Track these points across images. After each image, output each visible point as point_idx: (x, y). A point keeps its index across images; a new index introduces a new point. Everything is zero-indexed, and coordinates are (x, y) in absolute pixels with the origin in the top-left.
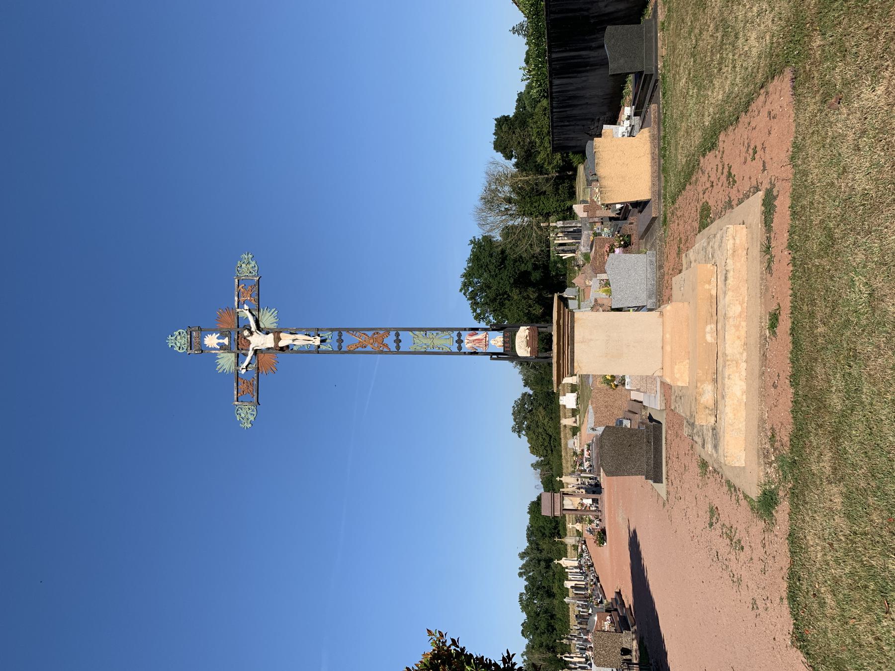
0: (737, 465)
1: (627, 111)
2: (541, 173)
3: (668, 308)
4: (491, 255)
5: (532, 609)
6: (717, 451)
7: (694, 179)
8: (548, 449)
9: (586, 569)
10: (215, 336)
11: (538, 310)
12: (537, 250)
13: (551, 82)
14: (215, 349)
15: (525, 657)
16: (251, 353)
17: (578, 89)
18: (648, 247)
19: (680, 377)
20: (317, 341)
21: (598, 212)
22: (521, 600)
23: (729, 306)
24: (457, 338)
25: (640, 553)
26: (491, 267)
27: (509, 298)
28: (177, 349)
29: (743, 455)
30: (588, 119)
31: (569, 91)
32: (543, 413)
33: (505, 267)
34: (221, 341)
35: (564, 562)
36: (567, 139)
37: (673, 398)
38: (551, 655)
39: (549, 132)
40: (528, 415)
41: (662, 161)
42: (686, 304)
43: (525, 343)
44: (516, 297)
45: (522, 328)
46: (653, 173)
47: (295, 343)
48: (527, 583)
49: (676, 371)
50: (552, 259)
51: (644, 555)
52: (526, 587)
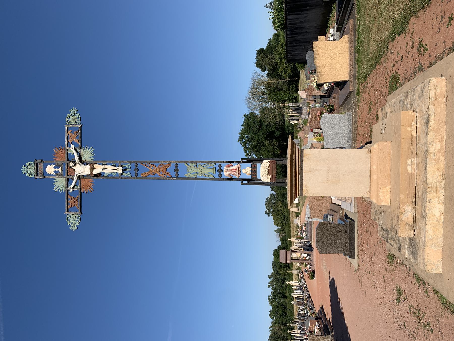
0: (435, 272)
1: (332, 31)
2: (281, 79)
3: (375, 146)
4: (254, 123)
5: (275, 304)
6: (415, 258)
7: (383, 59)
8: (284, 222)
9: (303, 288)
10: (53, 166)
11: (279, 152)
12: (279, 120)
13: (286, 18)
14: (53, 175)
15: (271, 329)
16: (75, 178)
17: (302, 22)
18: (346, 110)
19: (383, 198)
20: (120, 170)
21: (313, 92)
22: (269, 299)
23: (430, 144)
24: (218, 168)
25: (337, 293)
26: (254, 129)
27: (264, 145)
28: (28, 175)
29: (440, 264)
30: (307, 42)
31: (296, 23)
32: (281, 204)
33: (261, 129)
34: (57, 170)
35: (291, 283)
36: (295, 55)
37: (373, 211)
38: (284, 327)
39: (285, 57)
40: (273, 205)
41: (357, 55)
42: (389, 143)
43: (267, 172)
44: (267, 145)
45: (265, 161)
46: (350, 63)
47: (104, 171)
48: (272, 291)
49: (380, 194)
50: (286, 125)
51: (340, 295)
52: (272, 292)
